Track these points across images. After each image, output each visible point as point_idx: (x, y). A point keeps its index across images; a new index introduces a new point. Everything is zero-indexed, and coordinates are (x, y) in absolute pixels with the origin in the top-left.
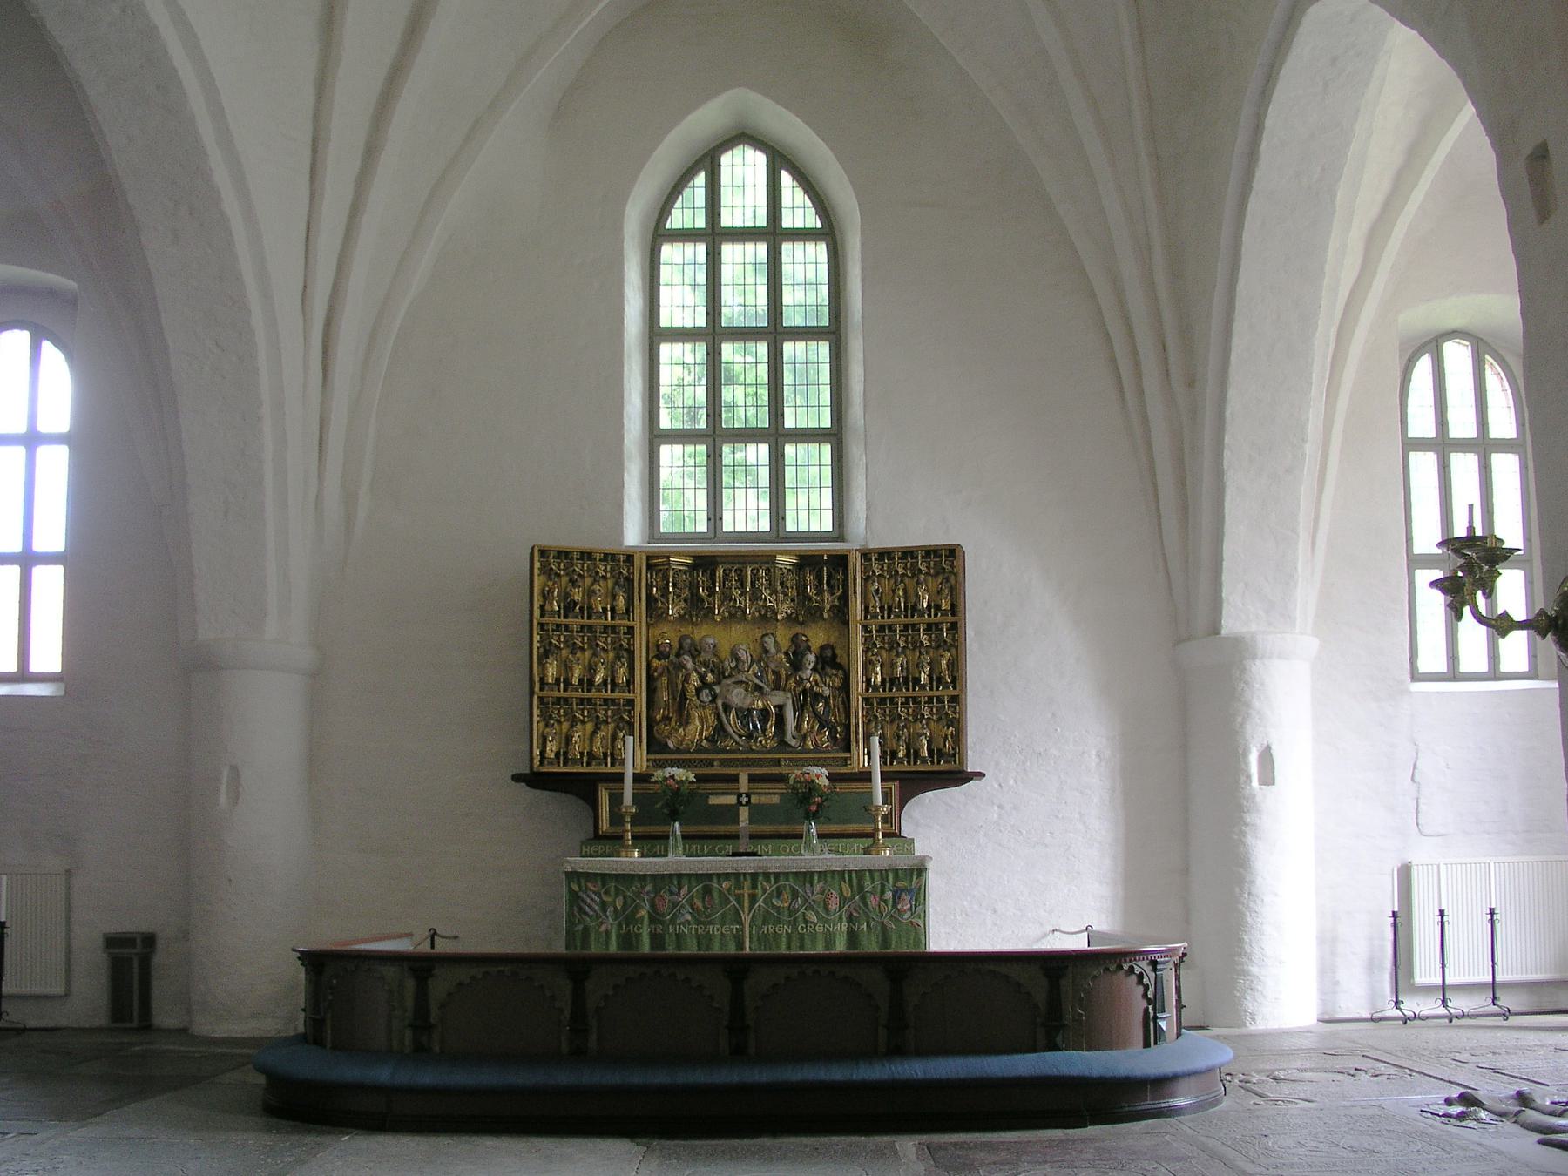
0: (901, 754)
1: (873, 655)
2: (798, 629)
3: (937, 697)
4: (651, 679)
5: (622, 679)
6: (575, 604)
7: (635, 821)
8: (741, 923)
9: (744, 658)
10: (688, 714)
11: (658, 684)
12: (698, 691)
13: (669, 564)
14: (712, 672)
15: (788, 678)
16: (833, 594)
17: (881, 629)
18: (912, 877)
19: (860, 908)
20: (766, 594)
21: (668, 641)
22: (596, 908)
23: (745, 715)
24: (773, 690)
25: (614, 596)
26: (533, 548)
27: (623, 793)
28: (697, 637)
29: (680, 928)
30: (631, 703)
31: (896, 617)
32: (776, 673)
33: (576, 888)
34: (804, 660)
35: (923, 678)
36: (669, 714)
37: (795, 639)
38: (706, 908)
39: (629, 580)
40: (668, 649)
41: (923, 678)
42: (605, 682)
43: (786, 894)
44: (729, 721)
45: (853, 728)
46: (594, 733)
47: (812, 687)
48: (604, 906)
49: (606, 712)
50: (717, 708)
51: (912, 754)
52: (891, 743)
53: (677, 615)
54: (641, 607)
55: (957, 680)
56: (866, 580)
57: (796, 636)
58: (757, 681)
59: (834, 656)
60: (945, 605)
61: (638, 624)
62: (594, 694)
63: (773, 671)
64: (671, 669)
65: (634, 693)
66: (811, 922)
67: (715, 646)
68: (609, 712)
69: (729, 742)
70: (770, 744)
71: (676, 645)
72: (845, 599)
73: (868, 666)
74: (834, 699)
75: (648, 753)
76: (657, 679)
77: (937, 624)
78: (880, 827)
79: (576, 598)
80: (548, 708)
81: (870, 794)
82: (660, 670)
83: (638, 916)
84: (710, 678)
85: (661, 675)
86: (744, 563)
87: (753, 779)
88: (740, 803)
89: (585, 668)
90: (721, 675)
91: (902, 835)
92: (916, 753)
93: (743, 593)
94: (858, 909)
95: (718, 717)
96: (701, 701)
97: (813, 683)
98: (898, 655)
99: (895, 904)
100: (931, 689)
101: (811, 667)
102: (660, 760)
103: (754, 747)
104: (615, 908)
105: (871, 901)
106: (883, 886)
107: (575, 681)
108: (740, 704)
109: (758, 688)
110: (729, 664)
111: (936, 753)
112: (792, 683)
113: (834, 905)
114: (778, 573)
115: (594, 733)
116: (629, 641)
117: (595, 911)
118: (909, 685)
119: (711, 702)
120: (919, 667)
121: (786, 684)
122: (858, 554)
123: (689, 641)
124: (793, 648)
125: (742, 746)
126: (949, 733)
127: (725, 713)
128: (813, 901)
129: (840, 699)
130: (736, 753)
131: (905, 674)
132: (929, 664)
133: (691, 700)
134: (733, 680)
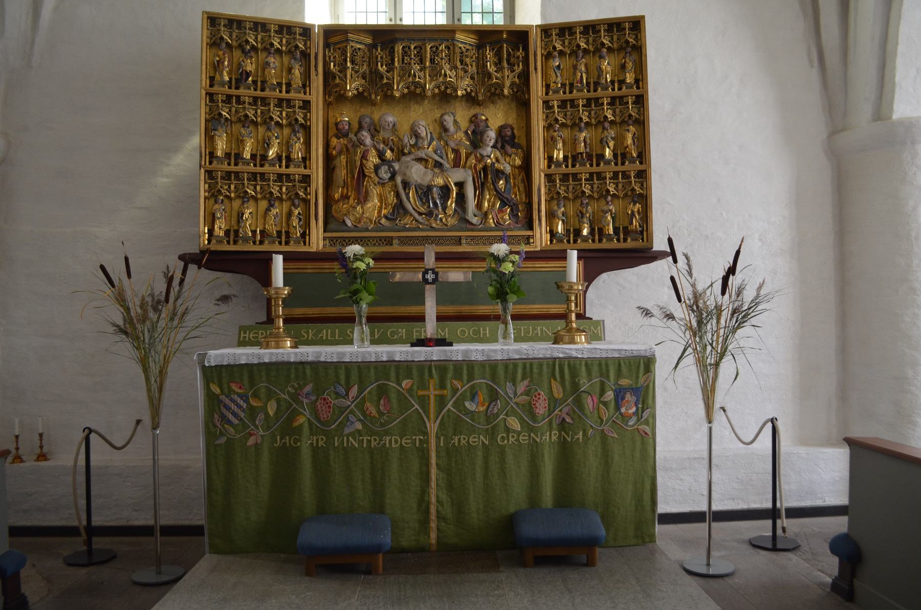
0: (585, 232)
1: (555, 131)
2: (475, 110)
3: (624, 173)
4: (328, 159)
5: (298, 152)
6: (248, 74)
7: (287, 302)
8: (425, 433)
9: (423, 134)
10: (367, 192)
11: (337, 162)
12: (377, 168)
13: (347, 40)
14: (392, 150)
15: (468, 156)
16: (513, 71)
18: (638, 373)
19: (574, 411)
20: (446, 68)
21: (347, 119)
22: (242, 415)
23: (425, 192)
24: (454, 167)
25: (290, 70)
27: (565, 271)
28: (376, 117)
29: (348, 440)
30: (306, 179)
31: (579, 91)
32: (456, 152)
33: (216, 389)
34: (485, 136)
35: (608, 153)
36: (347, 192)
37: (474, 120)
38: (381, 414)
40: (347, 127)
41: (608, 153)
42: (279, 157)
43: (482, 396)
44: (408, 198)
45: (535, 206)
46: (268, 210)
47: (493, 164)
48: (252, 412)
49: (281, 189)
50: (396, 186)
51: (598, 232)
52: (574, 221)
53: (355, 92)
54: (318, 81)
55: (643, 155)
56: (548, 56)
57: (475, 116)
58: (437, 158)
59: (513, 136)
60: (630, 78)
61: (315, 99)
62: (267, 168)
63: (453, 150)
64: (349, 146)
65: (310, 169)
66: (514, 431)
67: (394, 125)
68: (284, 189)
69: (407, 220)
70: (451, 221)
71: (355, 125)
72: (525, 77)
73: (550, 144)
74: (514, 178)
75: (325, 231)
76: (336, 157)
77: (621, 98)
78: (573, 309)
79: (249, 69)
80: (217, 183)
81: (564, 272)
82: (338, 148)
83: (296, 424)
84: (388, 154)
85: (340, 153)
86: (424, 40)
87: (440, 257)
88: (425, 281)
89: (258, 143)
90: (400, 153)
91: (587, 315)
92: (601, 231)
93: (423, 69)
94: (572, 413)
95: (398, 195)
96: (380, 178)
97: (494, 160)
98: (581, 130)
99: (618, 407)
100: (616, 164)
101: (491, 144)
102: (337, 238)
103: (434, 225)
104: (267, 414)
105: (589, 403)
106: (602, 384)
107: (247, 155)
108: (419, 181)
109: (438, 165)
110: (409, 141)
111: (624, 231)
113: (541, 408)
114: (458, 51)
115: (268, 210)
116: (305, 116)
117: (241, 420)
118: (592, 161)
119: (390, 179)
120: (603, 143)
121: (466, 162)
122: (539, 30)
123: (368, 120)
124: (473, 127)
125: (421, 223)
126: (636, 210)
127: (405, 189)
128: (517, 404)
129: (520, 178)
130: (416, 231)
131: (588, 150)
132: (613, 139)
133: (370, 177)
134: (412, 157)
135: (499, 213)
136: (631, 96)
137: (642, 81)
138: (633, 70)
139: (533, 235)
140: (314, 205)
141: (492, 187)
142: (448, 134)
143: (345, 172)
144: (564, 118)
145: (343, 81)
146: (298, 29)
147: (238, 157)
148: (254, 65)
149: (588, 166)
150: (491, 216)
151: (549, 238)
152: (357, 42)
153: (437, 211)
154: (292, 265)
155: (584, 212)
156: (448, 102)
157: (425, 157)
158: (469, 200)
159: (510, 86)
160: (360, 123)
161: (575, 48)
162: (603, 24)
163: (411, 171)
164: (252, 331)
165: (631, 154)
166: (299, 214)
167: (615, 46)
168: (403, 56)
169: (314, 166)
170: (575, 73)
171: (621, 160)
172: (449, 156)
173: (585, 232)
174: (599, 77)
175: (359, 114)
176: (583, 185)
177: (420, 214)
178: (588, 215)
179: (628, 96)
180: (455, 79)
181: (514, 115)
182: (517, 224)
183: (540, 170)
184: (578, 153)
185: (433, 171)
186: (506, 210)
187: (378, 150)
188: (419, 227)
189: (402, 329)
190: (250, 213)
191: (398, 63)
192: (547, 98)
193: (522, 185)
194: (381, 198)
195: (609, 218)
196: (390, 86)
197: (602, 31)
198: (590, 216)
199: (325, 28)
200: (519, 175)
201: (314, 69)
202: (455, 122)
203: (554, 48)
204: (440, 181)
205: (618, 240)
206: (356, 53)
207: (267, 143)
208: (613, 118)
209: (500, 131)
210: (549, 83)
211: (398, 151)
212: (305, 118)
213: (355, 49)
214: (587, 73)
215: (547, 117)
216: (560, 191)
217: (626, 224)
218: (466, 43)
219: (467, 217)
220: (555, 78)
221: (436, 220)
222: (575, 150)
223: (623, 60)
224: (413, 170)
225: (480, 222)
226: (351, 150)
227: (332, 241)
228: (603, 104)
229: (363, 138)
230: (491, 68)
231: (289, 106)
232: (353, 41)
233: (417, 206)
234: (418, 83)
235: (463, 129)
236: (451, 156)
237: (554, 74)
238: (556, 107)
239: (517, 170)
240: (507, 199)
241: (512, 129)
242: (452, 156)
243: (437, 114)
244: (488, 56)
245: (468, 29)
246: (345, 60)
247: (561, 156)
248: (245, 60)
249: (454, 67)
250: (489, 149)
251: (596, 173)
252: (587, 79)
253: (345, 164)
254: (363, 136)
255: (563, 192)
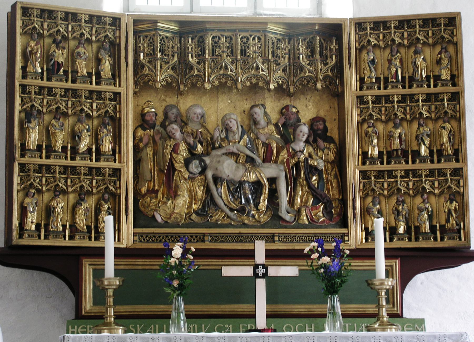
0: (401, 230)
2: (286, 101)
4: (137, 149)
6: (59, 65)
9: (235, 128)
10: (177, 187)
11: (143, 154)
12: (187, 163)
13: (156, 29)
16: (326, 64)
17: (377, 100)
25: (99, 61)
26: (14, 7)
30: (117, 173)
34: (298, 130)
35: (424, 151)
37: (284, 111)
39: (115, 197)
41: (424, 151)
45: (350, 203)
53: (164, 83)
57: (286, 107)
58: (249, 153)
59: (326, 129)
60: (445, 75)
63: (264, 144)
64: (157, 138)
67: (202, 116)
71: (161, 116)
74: (327, 174)
75: (134, 227)
76: (142, 149)
79: (61, 60)
82: (145, 140)
84: (199, 149)
85: (146, 145)
86: (235, 30)
87: (270, 254)
92: (417, 229)
95: (208, 190)
96: (190, 173)
101: (304, 139)
103: (246, 222)
107: (58, 147)
108: (231, 176)
109: (250, 160)
112: (284, 154)
116: (115, 108)
120: (419, 139)
121: (277, 156)
129: (333, 173)
132: (428, 136)
133: (180, 171)
135: (312, 210)
136: (446, 93)
137: (458, 78)
138: (449, 67)
139: (348, 233)
140: (124, 200)
141: (305, 182)
142: (258, 127)
143: (152, 165)
144: (378, 114)
145: (152, 71)
146: (108, 19)
147: (50, 150)
148: (65, 56)
149: (404, 163)
150: (304, 213)
151: (364, 236)
152: (165, 31)
153: (249, 207)
154: (123, 261)
155: (400, 210)
156: (255, 93)
157: (237, 152)
158: (282, 196)
159: (323, 79)
160: (166, 114)
161: (389, 43)
162: (418, 19)
163: (223, 167)
164: (80, 326)
165: (448, 151)
166: (109, 208)
167: (430, 41)
168: (213, 46)
169: (124, 159)
170: (389, 68)
171: (437, 157)
172: (260, 150)
173: (401, 230)
174: (414, 72)
175: (164, 104)
176: (399, 182)
177: (232, 210)
178: (404, 213)
179: (443, 93)
180: (267, 73)
181: (326, 107)
182: (332, 221)
183: (355, 167)
184: (394, 150)
185: (245, 166)
186: (320, 206)
187: (188, 144)
188: (231, 224)
189: (242, 323)
190: (62, 207)
191: (209, 55)
192: (361, 93)
193: (335, 180)
194: (192, 193)
195: (426, 216)
196: (201, 78)
197: (417, 27)
198: (406, 214)
199: (135, 18)
200: (332, 170)
201: (124, 60)
202: (265, 113)
203: (369, 41)
204: (252, 177)
205: (435, 239)
206: (164, 41)
207: (78, 136)
208: (428, 115)
209: (313, 123)
210: (363, 76)
211: (207, 145)
212: (115, 111)
213: (163, 38)
214: (402, 68)
215: (361, 111)
216: (375, 188)
217: (443, 222)
218: (277, 34)
219: (280, 214)
220: (369, 73)
221: (248, 215)
222: (391, 146)
223: (439, 56)
224: (225, 164)
225: (293, 219)
226: (160, 143)
227: (142, 236)
228: (418, 101)
229: (173, 131)
230: (303, 61)
231: (99, 98)
232: (161, 30)
233: (228, 201)
234: (230, 76)
235: (274, 122)
236: (261, 149)
237: (368, 68)
238: (370, 103)
239: (329, 165)
240: (321, 195)
241: (324, 121)
242: (263, 149)
243: (246, 106)
244: (301, 49)
245: (281, 21)
246: (154, 50)
247: (376, 152)
248: (57, 51)
249: (267, 60)
250: (302, 144)
251: (411, 170)
252: (402, 74)
253: (152, 157)
254: (173, 129)
255: (379, 189)
